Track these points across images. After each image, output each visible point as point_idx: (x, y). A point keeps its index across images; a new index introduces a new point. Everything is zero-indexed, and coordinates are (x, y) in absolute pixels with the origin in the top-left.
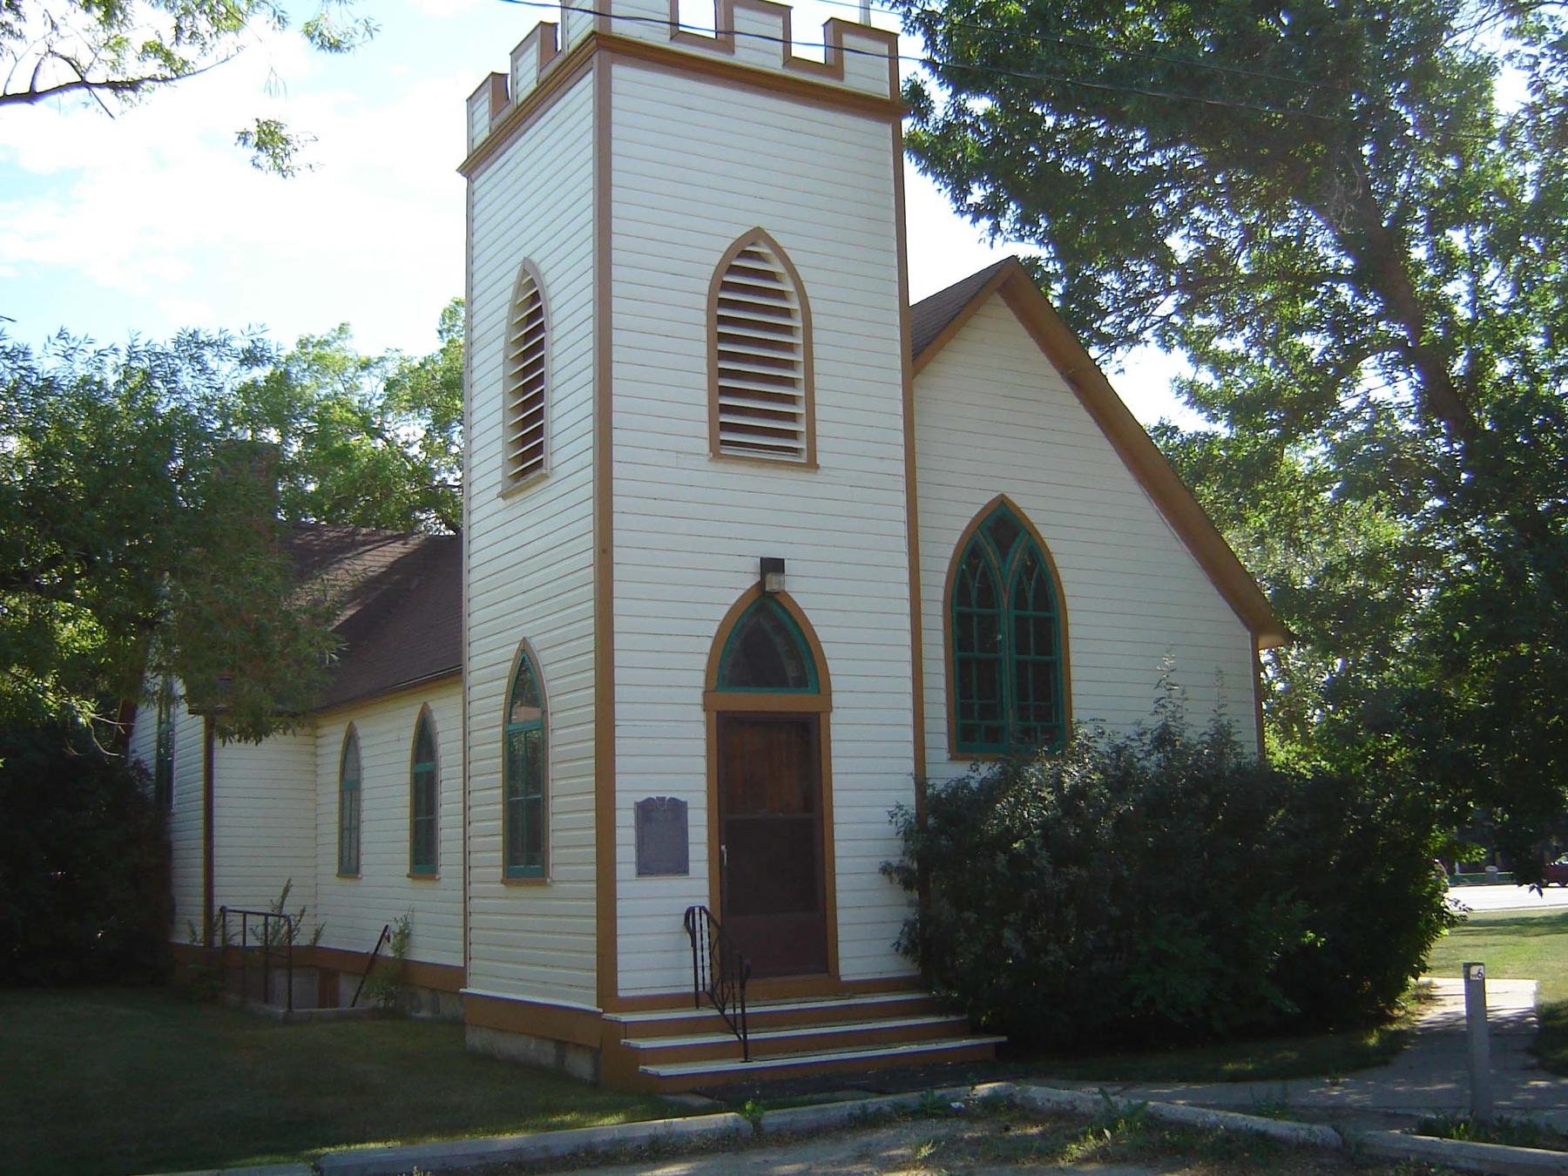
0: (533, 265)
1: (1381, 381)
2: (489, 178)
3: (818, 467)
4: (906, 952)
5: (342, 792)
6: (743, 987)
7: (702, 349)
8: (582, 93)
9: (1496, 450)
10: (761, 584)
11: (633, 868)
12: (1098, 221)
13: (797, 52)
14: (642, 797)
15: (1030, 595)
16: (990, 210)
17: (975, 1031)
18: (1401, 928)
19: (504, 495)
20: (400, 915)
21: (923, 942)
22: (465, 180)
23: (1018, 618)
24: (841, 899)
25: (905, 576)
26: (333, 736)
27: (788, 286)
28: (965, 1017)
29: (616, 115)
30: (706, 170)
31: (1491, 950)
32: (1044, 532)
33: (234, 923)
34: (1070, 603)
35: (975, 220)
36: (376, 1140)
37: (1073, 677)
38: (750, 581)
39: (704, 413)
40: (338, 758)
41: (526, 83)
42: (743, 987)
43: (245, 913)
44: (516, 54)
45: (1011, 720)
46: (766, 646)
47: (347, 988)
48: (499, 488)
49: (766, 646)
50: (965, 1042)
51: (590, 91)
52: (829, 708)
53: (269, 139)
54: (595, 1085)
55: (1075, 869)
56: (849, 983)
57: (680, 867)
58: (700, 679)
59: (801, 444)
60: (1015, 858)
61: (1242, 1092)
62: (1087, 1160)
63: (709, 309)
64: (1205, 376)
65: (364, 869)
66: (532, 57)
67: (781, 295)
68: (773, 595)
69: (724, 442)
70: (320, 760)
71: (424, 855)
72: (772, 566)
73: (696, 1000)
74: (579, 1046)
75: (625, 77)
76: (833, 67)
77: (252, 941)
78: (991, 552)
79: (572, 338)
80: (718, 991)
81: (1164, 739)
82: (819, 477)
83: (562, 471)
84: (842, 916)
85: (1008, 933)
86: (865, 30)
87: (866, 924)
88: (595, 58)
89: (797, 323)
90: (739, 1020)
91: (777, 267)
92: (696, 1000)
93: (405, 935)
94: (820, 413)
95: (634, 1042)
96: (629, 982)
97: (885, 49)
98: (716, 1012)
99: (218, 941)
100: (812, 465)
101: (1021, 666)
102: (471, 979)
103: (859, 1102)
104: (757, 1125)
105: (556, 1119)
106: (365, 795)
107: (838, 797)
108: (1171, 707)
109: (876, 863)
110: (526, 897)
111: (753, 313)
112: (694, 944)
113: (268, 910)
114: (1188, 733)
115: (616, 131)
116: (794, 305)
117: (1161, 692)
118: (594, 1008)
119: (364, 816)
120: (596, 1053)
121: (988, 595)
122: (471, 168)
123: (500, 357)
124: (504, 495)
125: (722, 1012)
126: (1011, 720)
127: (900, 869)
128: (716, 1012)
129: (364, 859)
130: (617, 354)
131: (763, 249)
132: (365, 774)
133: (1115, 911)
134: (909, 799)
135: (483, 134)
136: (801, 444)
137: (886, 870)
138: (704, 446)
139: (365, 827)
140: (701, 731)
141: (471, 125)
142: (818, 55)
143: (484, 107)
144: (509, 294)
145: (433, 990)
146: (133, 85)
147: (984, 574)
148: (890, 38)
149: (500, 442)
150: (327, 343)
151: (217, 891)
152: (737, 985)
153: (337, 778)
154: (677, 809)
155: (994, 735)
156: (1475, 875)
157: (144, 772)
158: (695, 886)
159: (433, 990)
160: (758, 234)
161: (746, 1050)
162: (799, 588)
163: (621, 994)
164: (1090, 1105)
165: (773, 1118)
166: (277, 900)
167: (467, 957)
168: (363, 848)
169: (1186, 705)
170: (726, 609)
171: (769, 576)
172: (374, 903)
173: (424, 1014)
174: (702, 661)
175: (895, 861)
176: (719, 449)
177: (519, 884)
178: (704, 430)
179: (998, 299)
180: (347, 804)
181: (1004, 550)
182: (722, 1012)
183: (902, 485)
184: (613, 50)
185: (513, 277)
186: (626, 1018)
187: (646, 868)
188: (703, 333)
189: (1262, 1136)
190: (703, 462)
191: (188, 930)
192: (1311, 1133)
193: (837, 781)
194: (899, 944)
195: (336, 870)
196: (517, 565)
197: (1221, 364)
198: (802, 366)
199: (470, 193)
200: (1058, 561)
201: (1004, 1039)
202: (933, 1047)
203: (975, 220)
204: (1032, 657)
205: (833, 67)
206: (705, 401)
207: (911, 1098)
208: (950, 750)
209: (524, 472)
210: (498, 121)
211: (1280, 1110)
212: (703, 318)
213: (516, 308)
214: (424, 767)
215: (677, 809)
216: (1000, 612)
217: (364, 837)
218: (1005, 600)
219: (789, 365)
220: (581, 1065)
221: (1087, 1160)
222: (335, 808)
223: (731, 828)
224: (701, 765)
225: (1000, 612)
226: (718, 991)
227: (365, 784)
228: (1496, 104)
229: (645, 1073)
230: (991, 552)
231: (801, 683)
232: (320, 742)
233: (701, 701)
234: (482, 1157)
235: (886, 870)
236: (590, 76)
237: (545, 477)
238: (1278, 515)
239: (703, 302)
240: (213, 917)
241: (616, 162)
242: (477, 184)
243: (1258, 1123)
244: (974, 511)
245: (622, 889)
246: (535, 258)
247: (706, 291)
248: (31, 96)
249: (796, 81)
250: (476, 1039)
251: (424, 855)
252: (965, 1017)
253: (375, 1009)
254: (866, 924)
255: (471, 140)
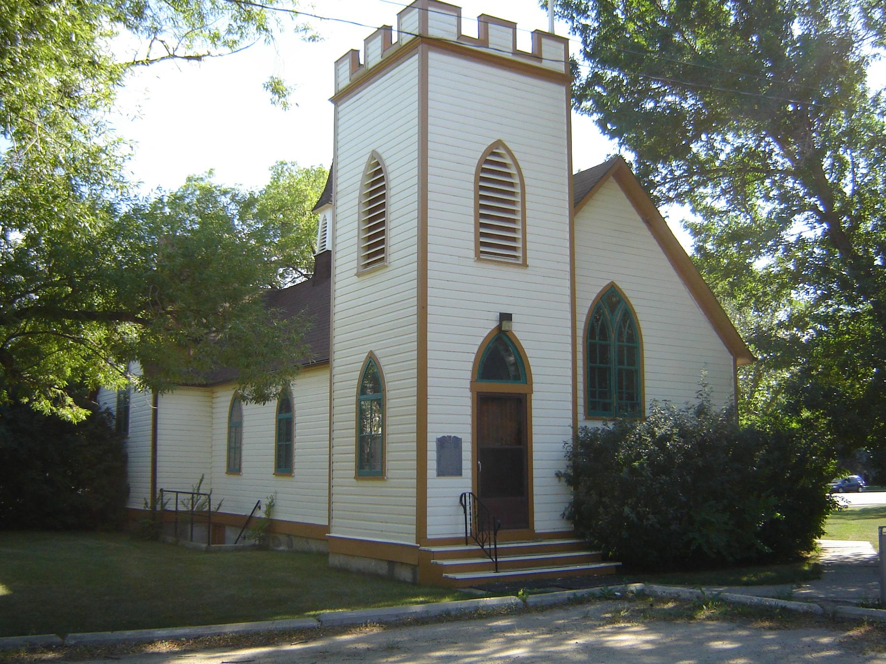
0: (377, 153)
1: (807, 228)
2: (347, 106)
3: (527, 266)
4: (568, 518)
5: (230, 428)
6: (495, 534)
7: (472, 203)
8: (412, 64)
9: (844, 262)
10: (499, 327)
11: (435, 472)
12: (658, 138)
13: (519, 47)
14: (440, 436)
15: (597, 331)
16: (613, 135)
17: (604, 559)
18: (812, 512)
19: (358, 275)
20: (269, 495)
21: (579, 516)
22: (333, 106)
23: (620, 346)
24: (536, 490)
25: (569, 324)
26: (224, 398)
27: (513, 171)
28: (601, 552)
29: (431, 79)
30: (475, 108)
31: (836, 526)
32: (633, 302)
33: (169, 498)
34: (645, 339)
35: (611, 138)
36: (329, 609)
37: (646, 378)
38: (494, 325)
39: (472, 236)
40: (228, 409)
41: (375, 57)
42: (495, 534)
43: (177, 492)
44: (367, 41)
45: (614, 399)
46: (500, 359)
47: (231, 534)
48: (355, 271)
49: (500, 359)
50: (603, 565)
51: (416, 64)
52: (531, 392)
53: (276, 88)
54: (414, 583)
55: (664, 477)
56: (541, 534)
57: (458, 472)
58: (469, 375)
59: (519, 254)
60: (633, 471)
61: (771, 589)
62: (709, 618)
63: (476, 183)
64: (698, 219)
65: (244, 470)
66: (378, 42)
67: (509, 175)
68: (505, 332)
69: (482, 252)
70: (214, 411)
71: (284, 461)
72: (506, 317)
73: (466, 541)
74: (402, 563)
75: (436, 59)
76: (483, 40)
77: (181, 508)
78: (607, 311)
79: (403, 195)
80: (480, 536)
81: (701, 411)
82: (529, 270)
83: (395, 265)
84: (536, 499)
85: (627, 509)
86: (551, 36)
87: (548, 503)
88: (420, 48)
89: (518, 190)
90: (493, 552)
91: (508, 161)
92: (466, 541)
93: (271, 506)
94: (529, 238)
95: (439, 562)
96: (434, 530)
97: (511, 30)
98: (479, 547)
99: (158, 507)
100: (525, 265)
101: (620, 372)
102: (333, 529)
103: (36, 656)
104: (524, 601)
105: (413, 600)
106: (245, 430)
107: (535, 438)
108: (705, 395)
109: (552, 473)
110: (370, 487)
111: (496, 183)
112: (465, 512)
113: (191, 491)
114: (713, 409)
115: (430, 87)
116: (516, 180)
117: (700, 388)
118: (414, 544)
119: (244, 441)
120: (414, 568)
121: (604, 334)
122: (338, 98)
123: (356, 201)
124: (358, 275)
125: (482, 547)
126: (614, 399)
127: (566, 475)
128: (479, 547)
129: (244, 465)
130: (430, 204)
131: (501, 151)
132: (245, 418)
133: (683, 499)
134: (569, 438)
135: (345, 82)
136: (519, 254)
137: (558, 475)
138: (472, 254)
139: (244, 447)
140: (469, 402)
141: (337, 76)
142: (529, 50)
143: (346, 67)
144: (363, 168)
145: (289, 535)
146: (198, 58)
147: (602, 324)
148: (565, 41)
149: (356, 246)
150: (202, 179)
151: (158, 480)
152: (492, 533)
153: (227, 420)
154: (457, 442)
155: (606, 408)
156: (852, 488)
157: (110, 414)
158: (465, 483)
159: (289, 535)
160: (499, 143)
161: (496, 566)
162: (519, 330)
163: (429, 537)
164: (688, 594)
165: (532, 599)
166: (196, 486)
167: (330, 518)
168: (243, 458)
169: (711, 394)
170: (482, 339)
171: (504, 323)
172: (251, 489)
173: (282, 548)
174: (470, 366)
175: (563, 471)
176: (479, 254)
177: (362, 479)
178: (472, 245)
179: (612, 179)
180: (233, 434)
181: (612, 310)
182: (482, 547)
183: (568, 276)
184: (429, 44)
185: (366, 159)
186: (434, 549)
187: (441, 473)
188: (472, 195)
189: (784, 609)
190: (471, 262)
191: (140, 499)
192: (810, 607)
193: (535, 429)
194: (564, 514)
195: (225, 470)
196: (363, 313)
197: (709, 213)
198: (520, 213)
199: (336, 113)
200: (639, 317)
201: (620, 563)
202: (571, 568)
203: (611, 138)
204: (625, 367)
205: (483, 40)
206: (473, 230)
207: (596, 590)
208: (585, 415)
209: (369, 264)
210: (355, 76)
211: (790, 597)
212: (472, 187)
213: (366, 176)
214: (285, 416)
215: (457, 442)
216: (610, 343)
217: (244, 453)
218: (613, 336)
219: (513, 212)
220: (405, 574)
221: (709, 618)
222: (226, 436)
223: (482, 453)
224: (469, 420)
225: (610, 343)
226: (480, 536)
227: (245, 424)
228: (868, 85)
229: (446, 577)
230: (607, 311)
231: (517, 378)
232: (214, 400)
233: (469, 386)
234: (397, 616)
235: (558, 475)
236: (416, 57)
237: (386, 266)
238: (757, 300)
239: (472, 178)
240: (156, 493)
241: (431, 104)
242: (340, 108)
243: (782, 603)
244: (599, 290)
245: (430, 482)
246: (380, 151)
247: (474, 172)
248: (149, 62)
249: (519, 63)
250: (335, 560)
251: (284, 461)
252: (601, 552)
253: (254, 545)
254: (548, 503)
255: (337, 84)
